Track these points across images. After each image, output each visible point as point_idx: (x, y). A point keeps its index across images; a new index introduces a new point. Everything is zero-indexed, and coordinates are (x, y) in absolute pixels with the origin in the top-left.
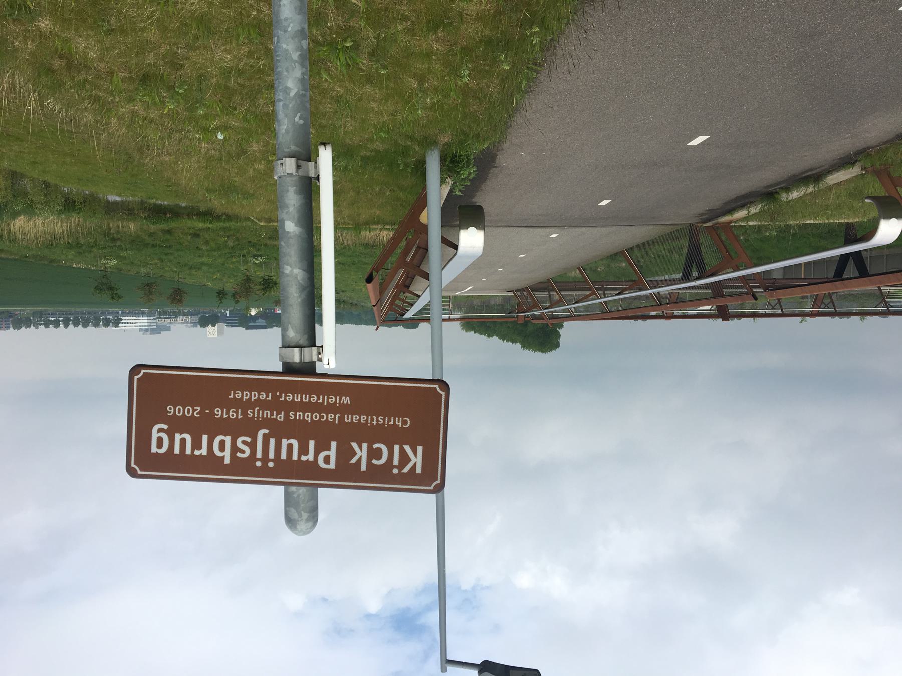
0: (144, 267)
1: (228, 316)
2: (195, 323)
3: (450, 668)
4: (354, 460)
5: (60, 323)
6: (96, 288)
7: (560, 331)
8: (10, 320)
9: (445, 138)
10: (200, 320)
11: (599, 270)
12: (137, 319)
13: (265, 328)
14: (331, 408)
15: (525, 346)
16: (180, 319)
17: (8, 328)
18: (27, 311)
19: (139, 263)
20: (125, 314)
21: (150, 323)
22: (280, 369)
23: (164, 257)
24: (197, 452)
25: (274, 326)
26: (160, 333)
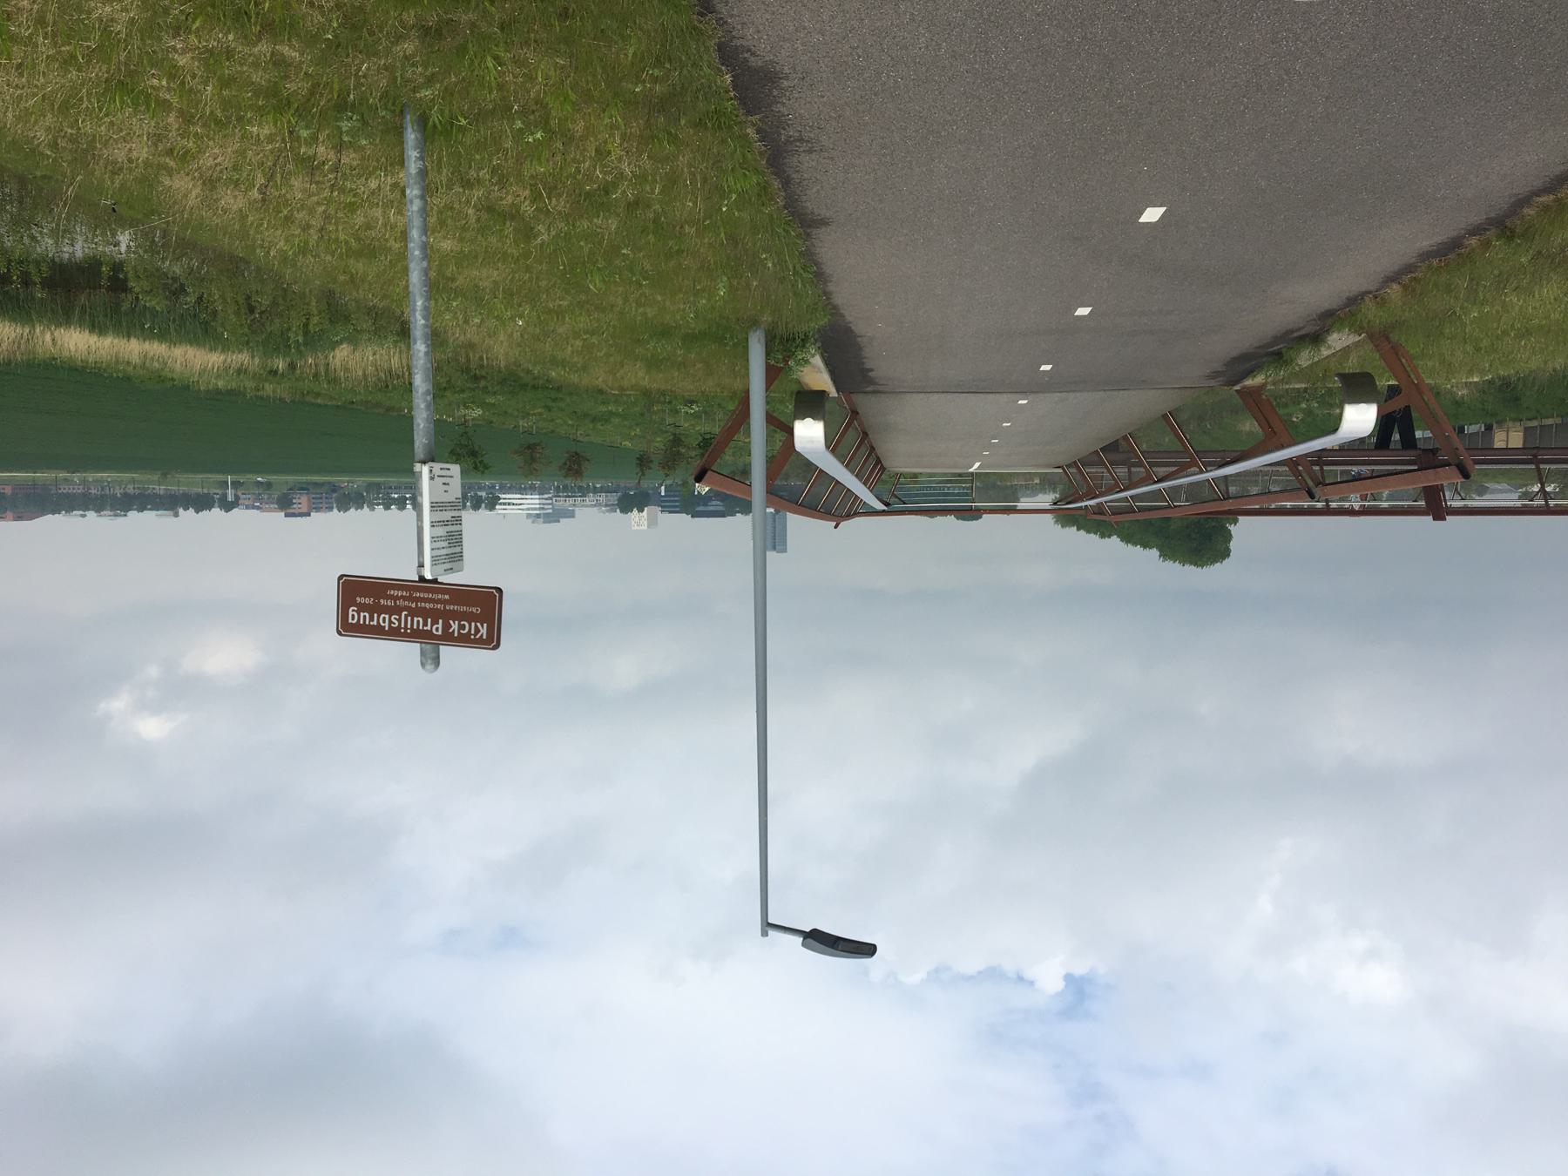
0: (523, 418)
1: (663, 494)
2: (613, 505)
3: (771, 933)
4: (451, 631)
5: (408, 502)
6: (452, 452)
7: (1232, 528)
8: (334, 495)
9: (767, 318)
10: (620, 500)
11: (1295, 419)
12: (523, 497)
13: (721, 514)
14: (439, 601)
15: (1167, 554)
16: (591, 497)
17: (331, 509)
18: (359, 482)
19: (516, 413)
20: (504, 490)
21: (543, 504)
22: (417, 579)
23: (550, 404)
24: (372, 623)
25: (738, 512)
26: (1444, 519)
